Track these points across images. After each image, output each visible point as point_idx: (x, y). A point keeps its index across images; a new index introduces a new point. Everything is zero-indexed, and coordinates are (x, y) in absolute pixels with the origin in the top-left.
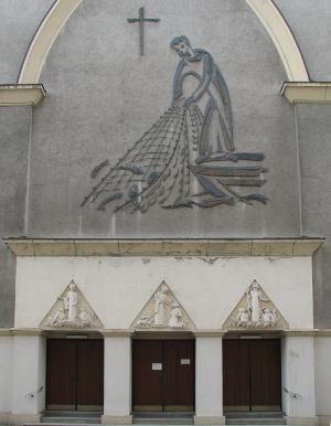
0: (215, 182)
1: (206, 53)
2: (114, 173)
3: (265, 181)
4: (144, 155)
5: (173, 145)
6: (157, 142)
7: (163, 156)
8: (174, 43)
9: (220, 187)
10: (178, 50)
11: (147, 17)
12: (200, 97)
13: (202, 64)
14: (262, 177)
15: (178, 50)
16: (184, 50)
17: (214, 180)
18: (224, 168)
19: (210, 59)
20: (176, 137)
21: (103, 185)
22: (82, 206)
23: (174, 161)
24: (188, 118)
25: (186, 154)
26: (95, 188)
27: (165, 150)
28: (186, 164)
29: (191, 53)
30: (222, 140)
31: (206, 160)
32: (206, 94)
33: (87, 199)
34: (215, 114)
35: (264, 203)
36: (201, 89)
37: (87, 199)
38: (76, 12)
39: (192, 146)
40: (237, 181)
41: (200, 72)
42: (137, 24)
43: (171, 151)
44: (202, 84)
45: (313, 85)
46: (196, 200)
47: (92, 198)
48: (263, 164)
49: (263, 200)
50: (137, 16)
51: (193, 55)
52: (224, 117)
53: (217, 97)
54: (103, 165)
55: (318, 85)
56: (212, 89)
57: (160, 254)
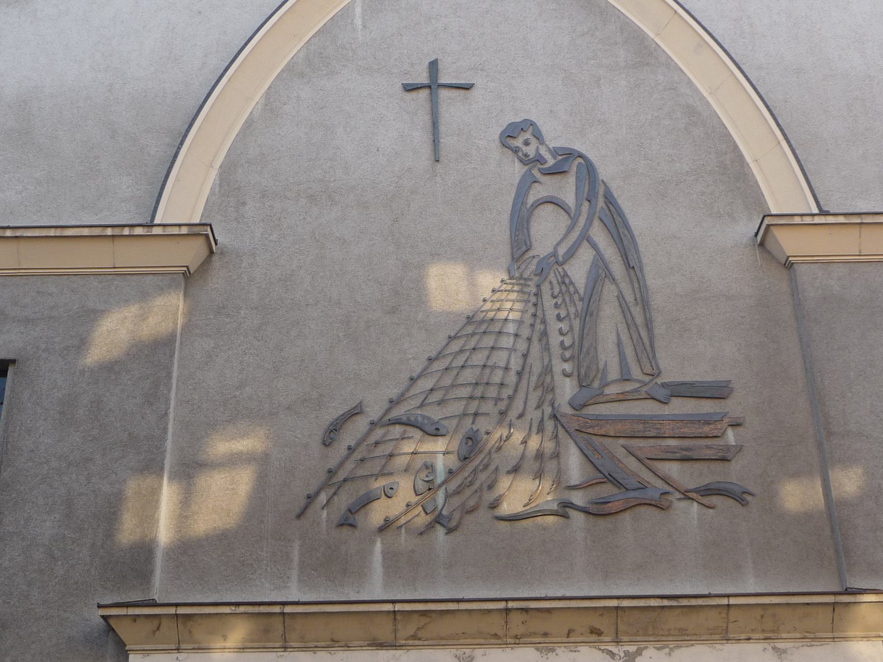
0: (620, 453)
1: (581, 156)
2: (379, 433)
3: (739, 449)
4: (448, 389)
5: (515, 363)
6: (479, 358)
7: (492, 392)
8: (509, 134)
9: (632, 464)
10: (516, 151)
11: (443, 80)
12: (571, 253)
13: (571, 179)
14: (731, 437)
15: (516, 151)
16: (531, 151)
17: (617, 447)
18: (643, 420)
19: (589, 170)
20: (522, 346)
21: (349, 466)
22: (299, 516)
23: (518, 405)
24: (548, 302)
25: (547, 388)
26: (331, 472)
27: (497, 377)
28: (548, 410)
29: (547, 156)
30: (629, 352)
31: (599, 398)
32: (585, 244)
33: (311, 498)
34: (609, 291)
35: (743, 502)
36: (575, 235)
37: (311, 498)
38: (289, 68)
39: (559, 366)
40: (668, 450)
41: (569, 198)
42: (424, 94)
43: (512, 378)
44: (570, 230)
45: (831, 220)
46: (578, 498)
47: (323, 498)
48: (732, 407)
49: (740, 497)
50: (424, 79)
51: (551, 162)
52: (629, 298)
53: (610, 252)
54: (356, 412)
55: (842, 219)
56: (598, 234)
57: (528, 230)
